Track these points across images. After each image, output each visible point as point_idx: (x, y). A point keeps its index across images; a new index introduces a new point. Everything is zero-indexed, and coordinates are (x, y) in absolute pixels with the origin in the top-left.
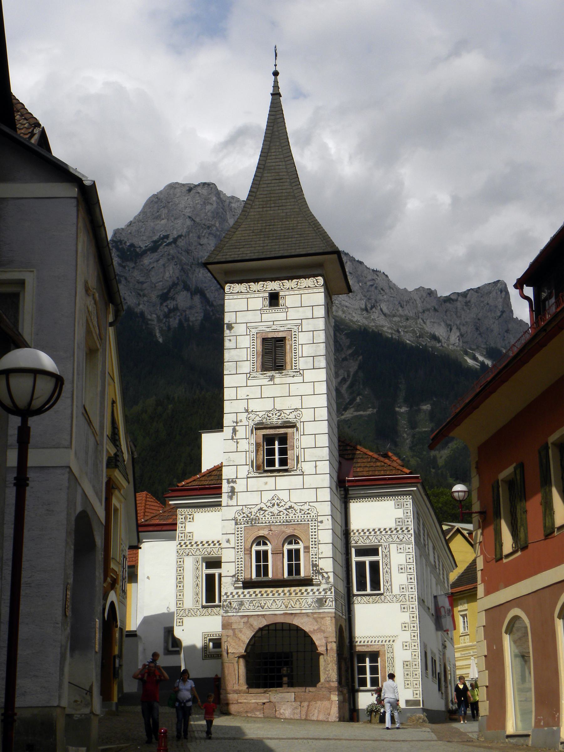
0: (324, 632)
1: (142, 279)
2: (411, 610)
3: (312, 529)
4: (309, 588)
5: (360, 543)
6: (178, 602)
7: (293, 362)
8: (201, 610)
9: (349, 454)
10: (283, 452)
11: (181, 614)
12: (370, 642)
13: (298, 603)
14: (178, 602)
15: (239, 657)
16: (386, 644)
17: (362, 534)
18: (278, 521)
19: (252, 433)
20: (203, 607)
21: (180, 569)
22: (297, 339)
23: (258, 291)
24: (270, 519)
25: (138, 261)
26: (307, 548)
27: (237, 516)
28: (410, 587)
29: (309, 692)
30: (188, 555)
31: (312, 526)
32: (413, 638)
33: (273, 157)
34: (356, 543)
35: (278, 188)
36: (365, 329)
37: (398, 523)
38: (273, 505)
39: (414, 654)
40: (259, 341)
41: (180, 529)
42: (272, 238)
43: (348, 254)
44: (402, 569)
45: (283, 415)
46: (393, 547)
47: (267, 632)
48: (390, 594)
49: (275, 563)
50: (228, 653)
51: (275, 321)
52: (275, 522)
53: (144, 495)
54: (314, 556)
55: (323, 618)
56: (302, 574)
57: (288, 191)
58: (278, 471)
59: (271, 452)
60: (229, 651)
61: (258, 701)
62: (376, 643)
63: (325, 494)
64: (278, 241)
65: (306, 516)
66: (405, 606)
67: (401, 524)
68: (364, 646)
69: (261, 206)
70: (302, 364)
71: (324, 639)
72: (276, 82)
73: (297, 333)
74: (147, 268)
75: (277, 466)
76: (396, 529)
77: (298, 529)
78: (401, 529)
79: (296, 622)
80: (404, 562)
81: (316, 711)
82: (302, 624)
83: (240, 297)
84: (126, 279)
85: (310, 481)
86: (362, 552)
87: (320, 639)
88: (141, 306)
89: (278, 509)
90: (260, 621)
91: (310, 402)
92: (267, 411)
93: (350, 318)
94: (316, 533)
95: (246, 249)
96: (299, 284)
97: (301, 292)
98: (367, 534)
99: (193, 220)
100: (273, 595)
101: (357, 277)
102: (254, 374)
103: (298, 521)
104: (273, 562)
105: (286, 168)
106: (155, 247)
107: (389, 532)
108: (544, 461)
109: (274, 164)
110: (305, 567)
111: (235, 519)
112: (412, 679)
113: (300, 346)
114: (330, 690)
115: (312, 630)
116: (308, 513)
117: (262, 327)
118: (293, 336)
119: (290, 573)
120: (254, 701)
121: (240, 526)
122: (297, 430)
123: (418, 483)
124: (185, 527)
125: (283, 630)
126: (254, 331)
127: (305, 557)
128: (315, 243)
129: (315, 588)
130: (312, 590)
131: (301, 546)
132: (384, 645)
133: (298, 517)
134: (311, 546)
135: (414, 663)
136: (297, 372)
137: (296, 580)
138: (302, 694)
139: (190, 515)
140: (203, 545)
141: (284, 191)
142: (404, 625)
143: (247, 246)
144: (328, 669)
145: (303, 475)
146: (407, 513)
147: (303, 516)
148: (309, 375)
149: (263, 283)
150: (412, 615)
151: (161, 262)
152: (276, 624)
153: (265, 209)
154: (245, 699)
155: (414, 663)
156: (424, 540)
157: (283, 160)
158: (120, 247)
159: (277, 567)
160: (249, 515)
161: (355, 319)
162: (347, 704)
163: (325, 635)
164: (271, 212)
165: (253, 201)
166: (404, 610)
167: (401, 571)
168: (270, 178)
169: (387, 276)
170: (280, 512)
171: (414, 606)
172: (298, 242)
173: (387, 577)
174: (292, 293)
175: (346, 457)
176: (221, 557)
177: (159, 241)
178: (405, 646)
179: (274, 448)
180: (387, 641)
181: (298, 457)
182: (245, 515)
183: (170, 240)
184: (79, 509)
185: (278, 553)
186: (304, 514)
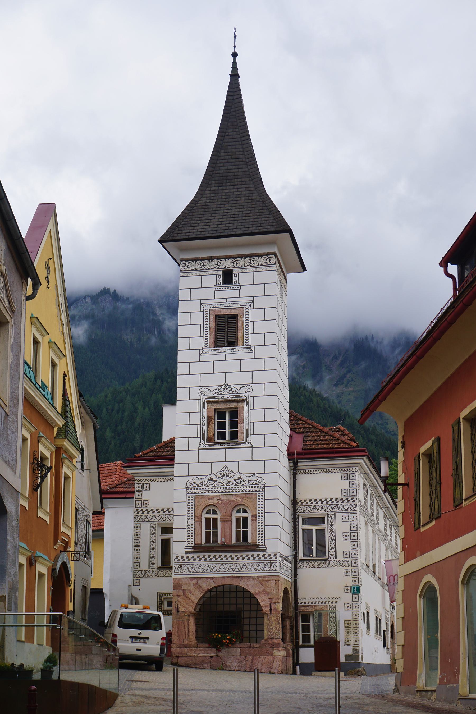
0: (268, 593)
2: (354, 574)
3: (259, 499)
4: (256, 554)
6: (136, 564)
7: (245, 338)
8: (157, 572)
9: (300, 428)
10: (234, 425)
11: (138, 575)
12: (314, 603)
13: (245, 567)
14: (136, 564)
15: (188, 615)
16: (329, 605)
17: (309, 503)
18: (227, 491)
19: (204, 407)
21: (137, 533)
22: (249, 316)
23: (212, 269)
24: (219, 489)
27: (188, 485)
28: (353, 553)
29: (254, 647)
30: (144, 521)
31: (259, 496)
32: (354, 600)
33: (231, 137)
34: (304, 512)
35: (234, 167)
37: (344, 494)
38: (223, 476)
39: (354, 614)
40: (212, 318)
42: (226, 217)
44: (346, 536)
45: (234, 390)
46: (339, 516)
47: (216, 593)
48: (334, 559)
49: (226, 528)
50: (178, 611)
51: (227, 298)
52: (224, 491)
54: (261, 524)
55: (267, 581)
56: (249, 541)
57: (243, 170)
58: (229, 443)
59: (222, 426)
60: (180, 610)
61: (205, 655)
65: (254, 486)
66: (348, 571)
67: (346, 494)
68: (308, 606)
69: (217, 185)
70: (255, 340)
72: (235, 63)
73: (249, 310)
76: (342, 499)
77: (246, 498)
78: (347, 499)
79: (243, 584)
80: (349, 531)
81: (260, 664)
82: (248, 586)
83: (194, 274)
86: (307, 521)
87: (264, 600)
89: (227, 479)
90: (208, 583)
92: (219, 386)
94: (263, 503)
95: (200, 227)
96: (252, 262)
98: (314, 503)
100: (222, 559)
102: (206, 350)
103: (246, 491)
104: (222, 529)
105: (242, 148)
107: (335, 503)
108: (456, 435)
109: (231, 144)
110: (252, 534)
114: (275, 646)
115: (257, 592)
117: (216, 305)
120: (201, 655)
121: (190, 495)
122: (247, 404)
123: (364, 456)
124: (142, 495)
125: (230, 591)
126: (207, 308)
127: (252, 525)
129: (261, 554)
130: (258, 555)
131: (248, 515)
132: (327, 606)
133: (246, 487)
134: (258, 515)
136: (249, 348)
138: (247, 649)
139: (147, 484)
140: (159, 512)
141: (240, 170)
142: (346, 588)
143: (202, 224)
144: (273, 627)
145: (252, 447)
146: (353, 484)
147: (251, 486)
149: (217, 261)
150: (354, 579)
152: (223, 585)
153: (221, 188)
154: (194, 653)
155: (355, 622)
156: (372, 509)
157: (239, 139)
162: (291, 659)
163: (270, 596)
164: (227, 191)
166: (347, 574)
167: (345, 538)
170: (229, 482)
172: (251, 220)
173: (332, 544)
174: (245, 270)
175: (297, 430)
179: (225, 422)
180: (330, 603)
181: (247, 431)
182: (195, 485)
186: (252, 484)
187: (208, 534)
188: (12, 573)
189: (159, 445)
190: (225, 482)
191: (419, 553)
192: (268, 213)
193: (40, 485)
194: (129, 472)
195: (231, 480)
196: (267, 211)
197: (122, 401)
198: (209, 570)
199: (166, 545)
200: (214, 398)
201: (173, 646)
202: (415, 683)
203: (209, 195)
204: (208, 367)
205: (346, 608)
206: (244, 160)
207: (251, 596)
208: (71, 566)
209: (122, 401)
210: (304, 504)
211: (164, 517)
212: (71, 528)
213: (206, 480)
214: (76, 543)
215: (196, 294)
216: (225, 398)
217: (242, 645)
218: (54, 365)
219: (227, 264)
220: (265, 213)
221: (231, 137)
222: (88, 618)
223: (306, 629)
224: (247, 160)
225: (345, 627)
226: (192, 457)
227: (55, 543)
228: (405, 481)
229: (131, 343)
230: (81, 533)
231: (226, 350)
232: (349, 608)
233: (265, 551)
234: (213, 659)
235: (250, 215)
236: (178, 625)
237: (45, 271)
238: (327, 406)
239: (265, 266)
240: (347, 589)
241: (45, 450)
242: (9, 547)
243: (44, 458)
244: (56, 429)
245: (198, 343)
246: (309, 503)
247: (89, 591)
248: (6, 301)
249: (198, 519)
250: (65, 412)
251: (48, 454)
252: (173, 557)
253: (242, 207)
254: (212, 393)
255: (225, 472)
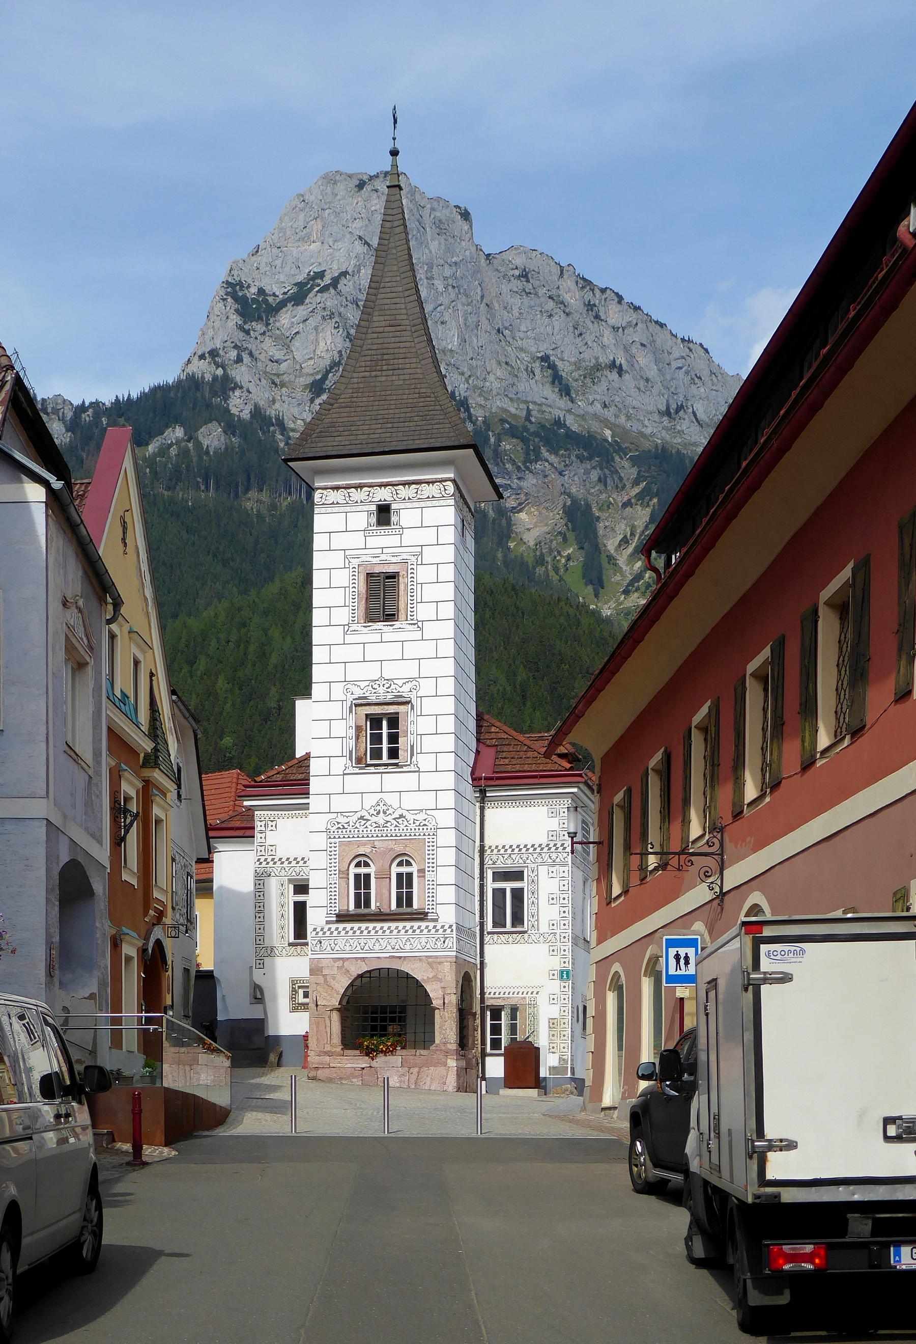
0: (441, 980)
1: (278, 355)
2: (563, 953)
4: (423, 924)
5: (499, 864)
10: (394, 738)
17: (502, 851)
19: (351, 711)
20: (290, 945)
25: (271, 322)
26: (421, 871)
33: (388, 290)
35: (393, 340)
36: (664, 449)
38: (378, 813)
39: (563, 1009)
40: (362, 577)
41: (259, 840)
43: (639, 308)
44: (553, 899)
45: (393, 686)
46: (543, 870)
49: (381, 892)
50: (317, 1006)
51: (383, 549)
53: (235, 776)
54: (431, 883)
55: (440, 963)
56: (415, 906)
57: (408, 344)
59: (376, 739)
62: (515, 995)
63: (449, 799)
64: (390, 425)
66: (555, 948)
69: (368, 369)
71: (442, 992)
73: (414, 567)
74: (288, 334)
75: (385, 759)
76: (547, 845)
78: (555, 845)
82: (413, 970)
84: (251, 354)
85: (428, 781)
88: (277, 405)
91: (429, 668)
93: (640, 428)
97: (422, 504)
98: (509, 851)
99: (366, 243)
101: (654, 353)
102: (354, 627)
106: (299, 296)
107: (538, 850)
109: (388, 301)
111: (327, 830)
112: (559, 1041)
113: (419, 586)
114: (447, 1053)
116: (425, 825)
118: (410, 571)
119: (399, 904)
120: (349, 1065)
121: (333, 841)
122: (412, 708)
126: (355, 562)
127: (419, 883)
128: (442, 430)
129: (431, 925)
130: (427, 927)
131: (414, 869)
134: (427, 869)
135: (563, 1021)
137: (407, 911)
140: (290, 863)
141: (402, 345)
143: (346, 433)
144: (446, 1027)
145: (419, 771)
148: (430, 630)
150: (563, 960)
151: (312, 322)
153: (374, 373)
155: (563, 1021)
158: (240, 294)
159: (384, 895)
160: (346, 826)
161: (648, 431)
163: (443, 985)
164: (383, 379)
165: (357, 360)
167: (551, 902)
168: (383, 324)
169: (706, 351)
170: (388, 822)
171: (566, 948)
173: (533, 910)
174: (409, 505)
175: (488, 742)
176: (308, 880)
177: (308, 283)
178: (552, 1000)
179: (382, 733)
181: (412, 747)
182: (340, 825)
183: (327, 280)
184: (65, 858)
185: (384, 876)
187: (357, 896)
188: (102, 966)
189: (290, 764)
190: (382, 822)
191: (609, 934)
192: (442, 417)
193: (123, 839)
194: (246, 803)
195: (389, 818)
196: (441, 412)
197: (244, 625)
198: (358, 948)
199: (300, 910)
200: (365, 698)
201: (310, 1053)
202: (601, 1101)
203: (356, 386)
204: (355, 653)
205: (552, 1002)
206: (408, 328)
207: (418, 985)
208: (168, 944)
209: (244, 625)
210: (495, 851)
211: (297, 870)
212: (166, 891)
213: (355, 818)
214: (173, 908)
215: (339, 541)
216: (381, 699)
217: (404, 1052)
218: (136, 663)
219: (383, 495)
220: (438, 417)
221: (388, 290)
222: (193, 1013)
223: (496, 1029)
224: (413, 329)
225: (550, 1027)
226: (334, 784)
227: (146, 913)
228: (600, 837)
229: (259, 515)
230: (179, 893)
231: (382, 627)
232: (555, 1002)
233: (436, 920)
234: (364, 1071)
235: (416, 419)
236: (318, 1024)
237: (121, 529)
238: (606, 634)
239: (439, 499)
240: (553, 975)
241: (129, 788)
242: (98, 936)
243: (127, 799)
244: (142, 755)
245: (342, 616)
246: (502, 851)
247: (193, 974)
248: (85, 639)
249: (344, 874)
250: (155, 731)
251: (133, 793)
252: (310, 929)
253: (405, 406)
254: (362, 692)
255: (381, 808)
